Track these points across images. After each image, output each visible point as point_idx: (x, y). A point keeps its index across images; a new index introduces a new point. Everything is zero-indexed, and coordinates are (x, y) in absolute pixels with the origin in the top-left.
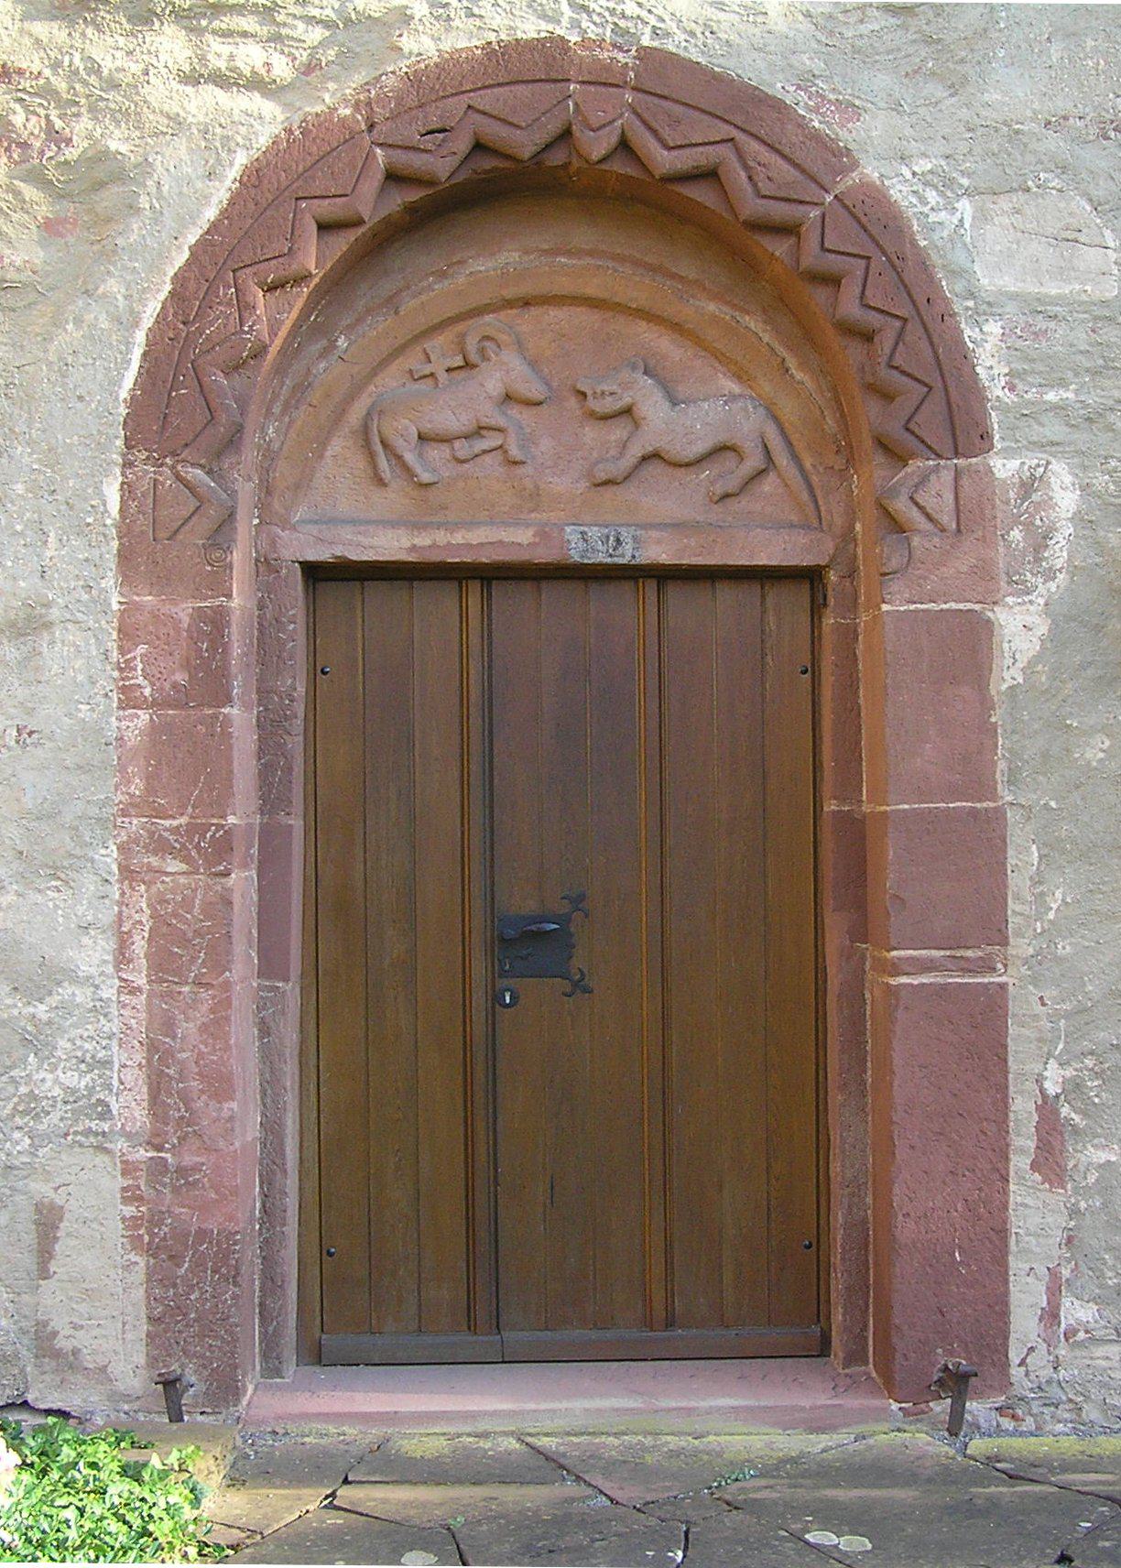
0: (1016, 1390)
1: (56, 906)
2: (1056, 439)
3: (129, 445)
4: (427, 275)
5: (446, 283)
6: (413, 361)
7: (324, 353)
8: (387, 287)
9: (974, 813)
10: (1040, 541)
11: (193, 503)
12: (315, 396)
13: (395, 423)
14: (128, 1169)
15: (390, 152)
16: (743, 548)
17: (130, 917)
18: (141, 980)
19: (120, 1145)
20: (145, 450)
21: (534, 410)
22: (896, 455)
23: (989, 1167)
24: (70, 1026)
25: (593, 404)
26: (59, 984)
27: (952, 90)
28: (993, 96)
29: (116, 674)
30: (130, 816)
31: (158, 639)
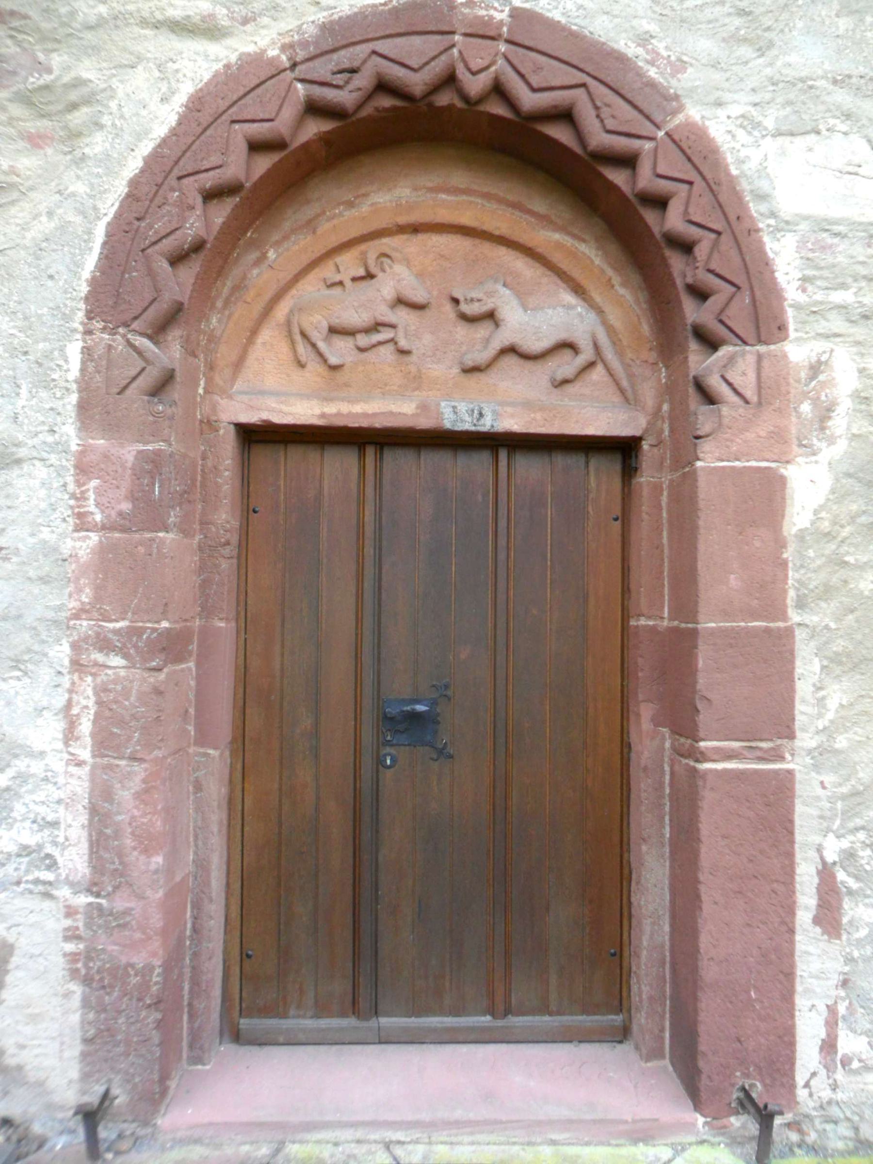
0: (805, 1110)
1: (17, 693)
2: (837, 331)
3: (90, 315)
4: (339, 204)
5: (353, 211)
6: (327, 271)
7: (258, 262)
8: (309, 212)
9: (767, 630)
10: (825, 413)
11: (141, 364)
12: (250, 295)
13: (311, 318)
14: (70, 912)
15: (308, 86)
16: (577, 422)
17: (78, 703)
18: (85, 754)
19: (64, 892)
20: (103, 321)
21: (418, 313)
22: (711, 343)
23: (779, 920)
24: (26, 792)
25: (464, 308)
26: (16, 756)
27: (760, 53)
28: (793, 58)
29: (72, 502)
30: (80, 619)
31: (108, 475)
